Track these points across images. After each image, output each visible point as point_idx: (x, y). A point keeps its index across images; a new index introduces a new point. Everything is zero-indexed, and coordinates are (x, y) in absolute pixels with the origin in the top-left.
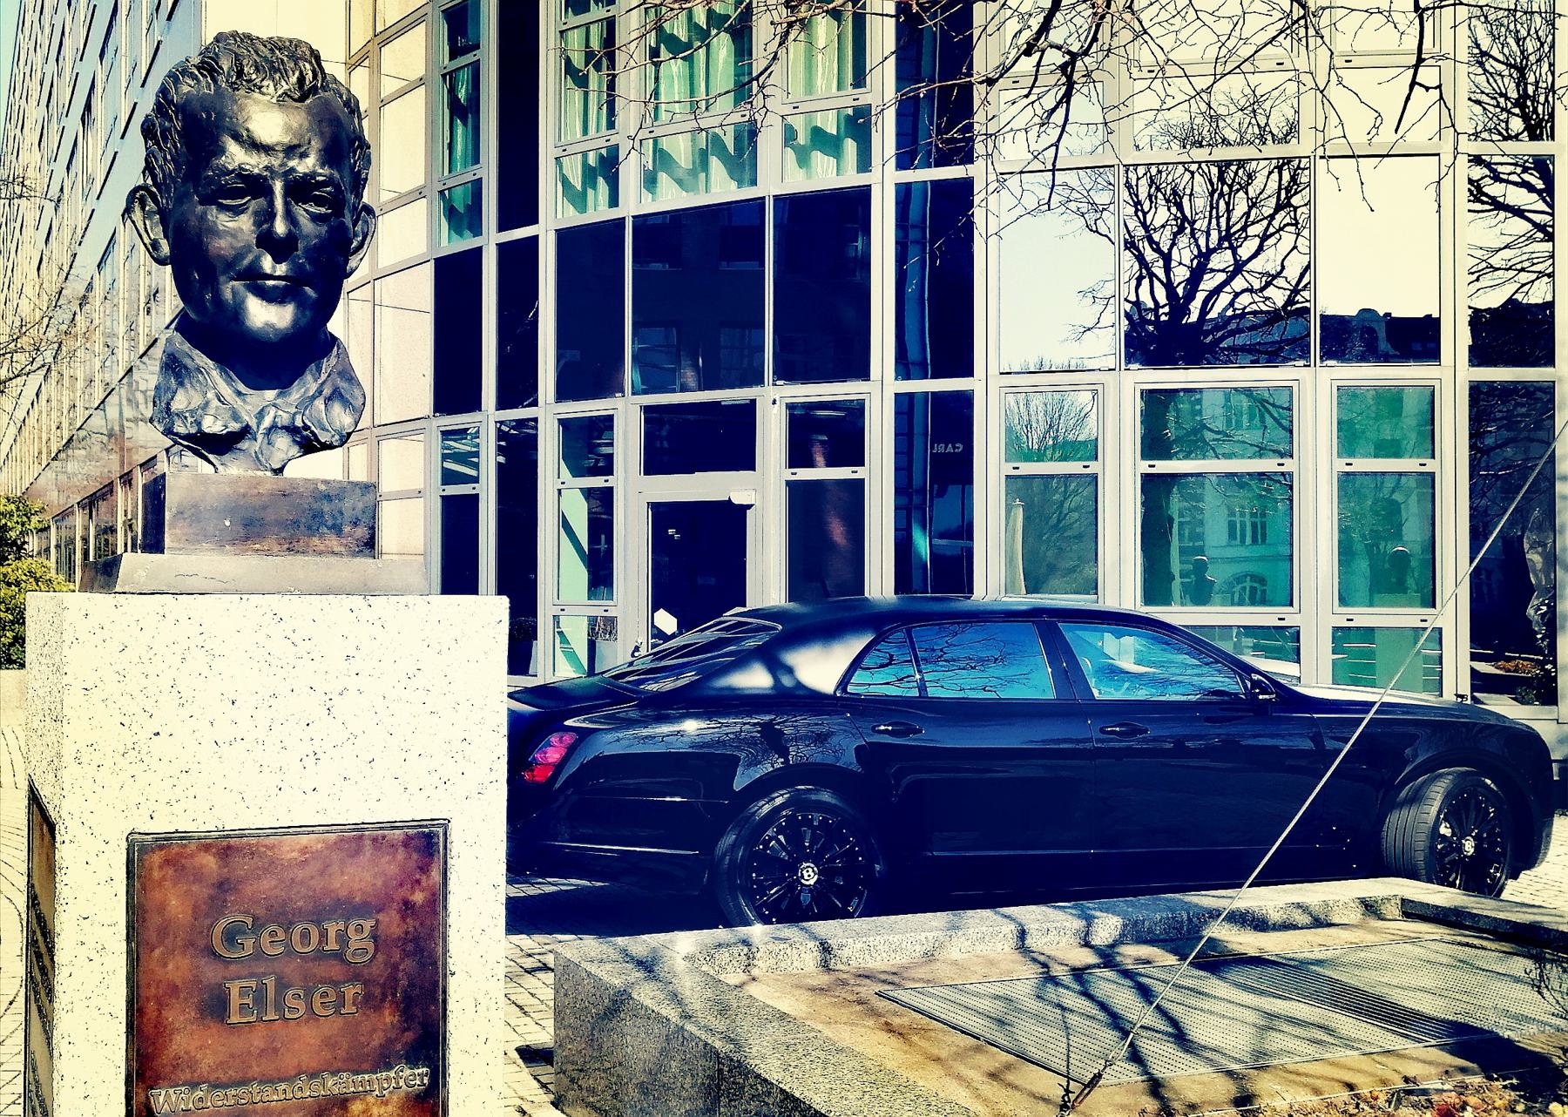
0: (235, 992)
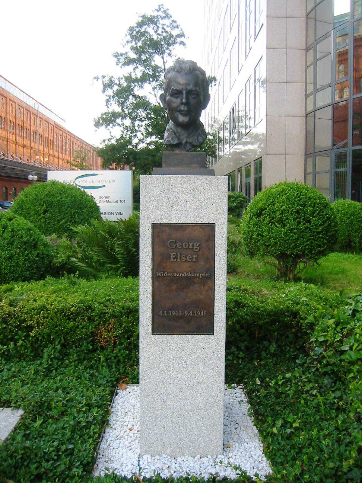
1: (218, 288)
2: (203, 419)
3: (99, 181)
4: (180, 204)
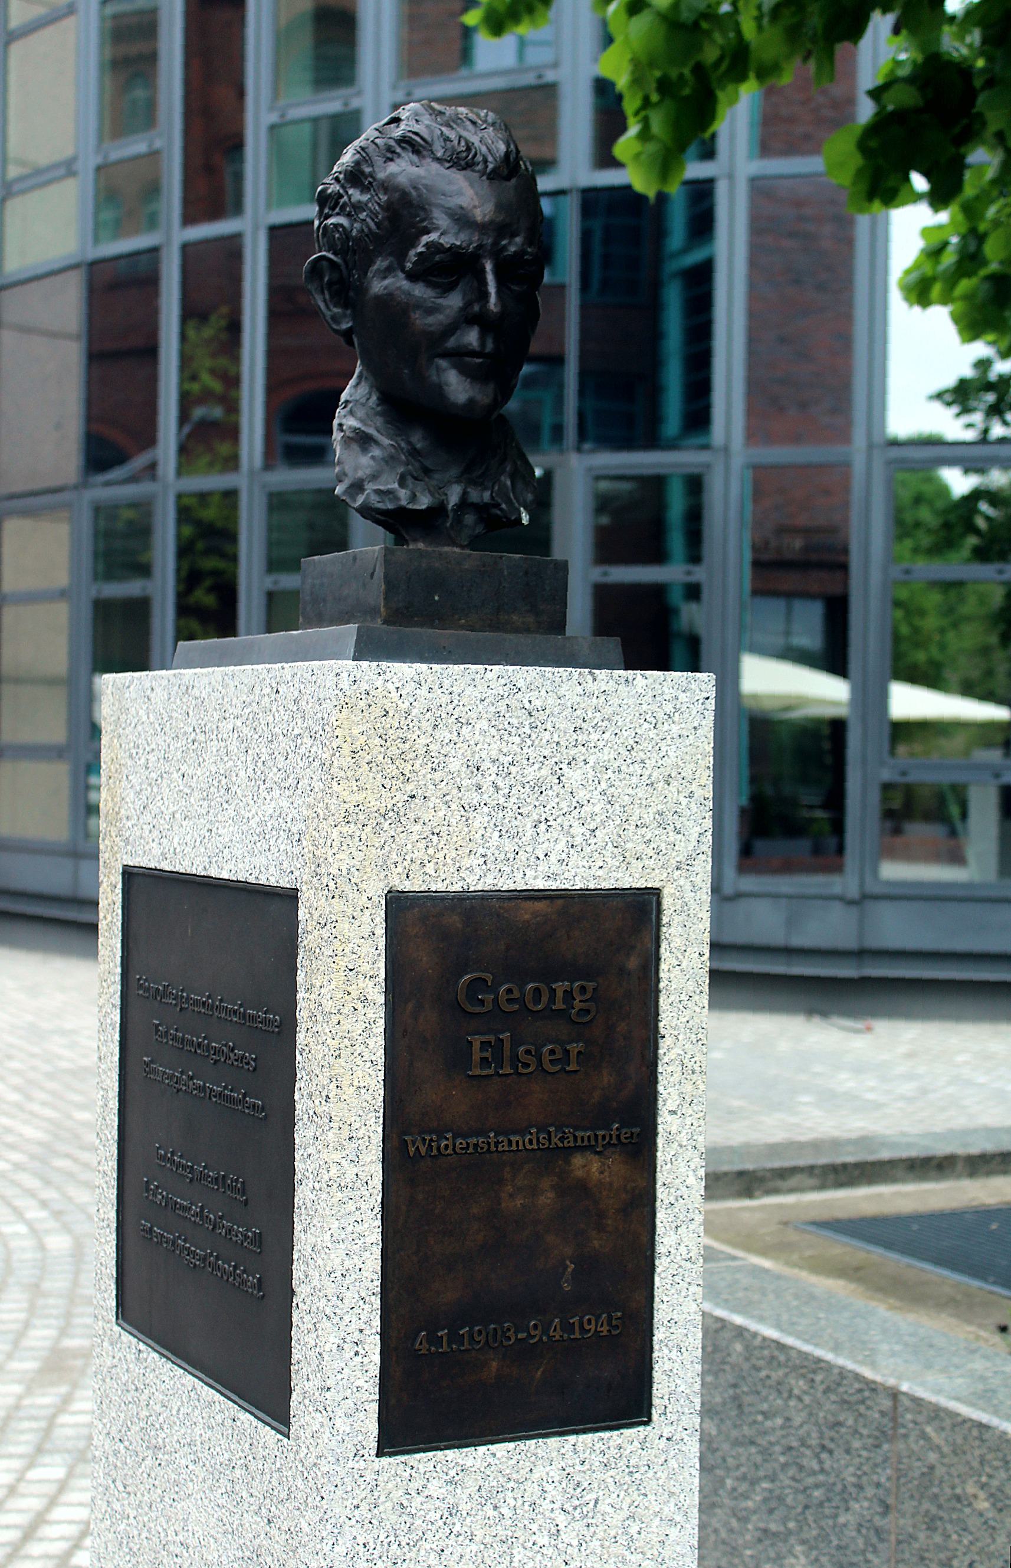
0: (476, 1046)
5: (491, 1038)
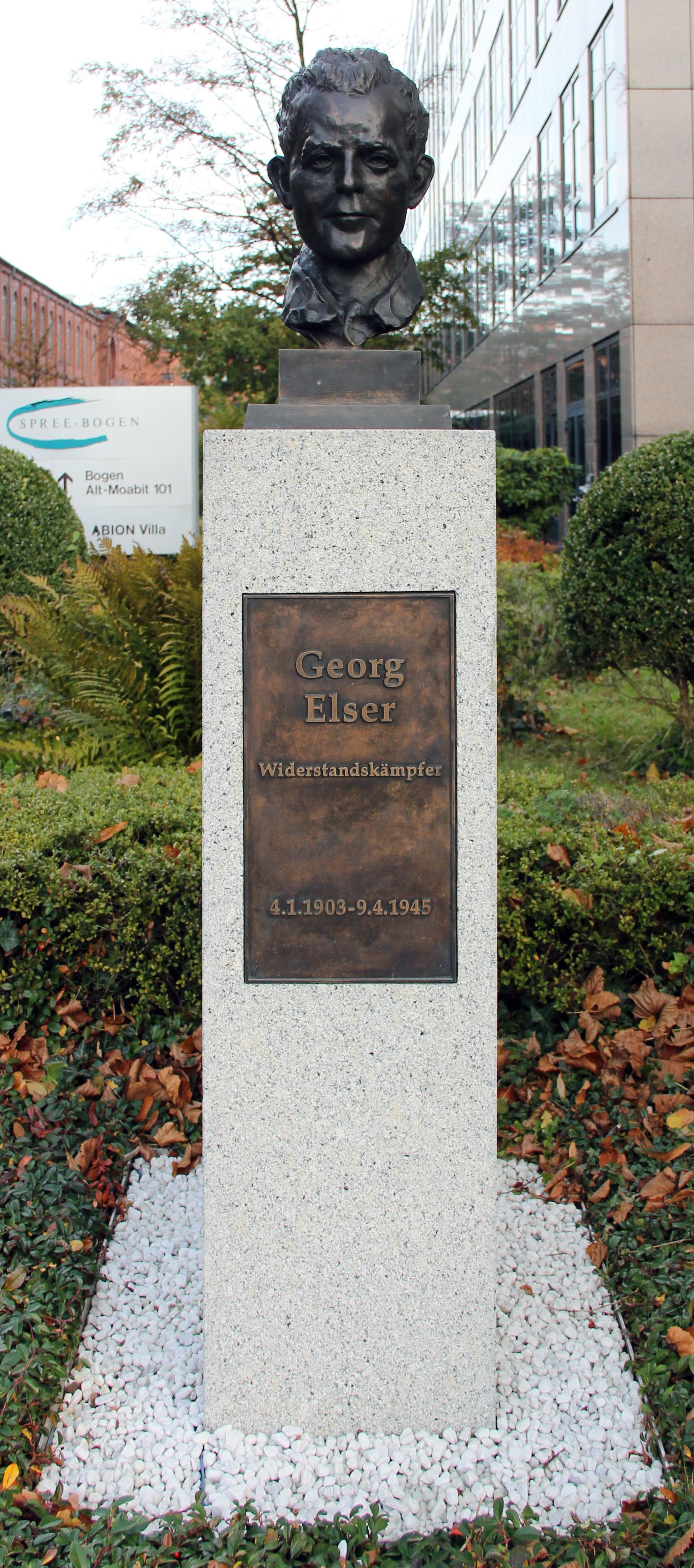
0: (311, 701)
1: (469, 818)
2: (424, 1290)
3: (86, 423)
4: (336, 524)
5: (323, 697)
